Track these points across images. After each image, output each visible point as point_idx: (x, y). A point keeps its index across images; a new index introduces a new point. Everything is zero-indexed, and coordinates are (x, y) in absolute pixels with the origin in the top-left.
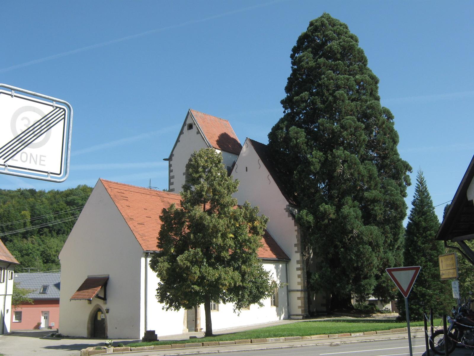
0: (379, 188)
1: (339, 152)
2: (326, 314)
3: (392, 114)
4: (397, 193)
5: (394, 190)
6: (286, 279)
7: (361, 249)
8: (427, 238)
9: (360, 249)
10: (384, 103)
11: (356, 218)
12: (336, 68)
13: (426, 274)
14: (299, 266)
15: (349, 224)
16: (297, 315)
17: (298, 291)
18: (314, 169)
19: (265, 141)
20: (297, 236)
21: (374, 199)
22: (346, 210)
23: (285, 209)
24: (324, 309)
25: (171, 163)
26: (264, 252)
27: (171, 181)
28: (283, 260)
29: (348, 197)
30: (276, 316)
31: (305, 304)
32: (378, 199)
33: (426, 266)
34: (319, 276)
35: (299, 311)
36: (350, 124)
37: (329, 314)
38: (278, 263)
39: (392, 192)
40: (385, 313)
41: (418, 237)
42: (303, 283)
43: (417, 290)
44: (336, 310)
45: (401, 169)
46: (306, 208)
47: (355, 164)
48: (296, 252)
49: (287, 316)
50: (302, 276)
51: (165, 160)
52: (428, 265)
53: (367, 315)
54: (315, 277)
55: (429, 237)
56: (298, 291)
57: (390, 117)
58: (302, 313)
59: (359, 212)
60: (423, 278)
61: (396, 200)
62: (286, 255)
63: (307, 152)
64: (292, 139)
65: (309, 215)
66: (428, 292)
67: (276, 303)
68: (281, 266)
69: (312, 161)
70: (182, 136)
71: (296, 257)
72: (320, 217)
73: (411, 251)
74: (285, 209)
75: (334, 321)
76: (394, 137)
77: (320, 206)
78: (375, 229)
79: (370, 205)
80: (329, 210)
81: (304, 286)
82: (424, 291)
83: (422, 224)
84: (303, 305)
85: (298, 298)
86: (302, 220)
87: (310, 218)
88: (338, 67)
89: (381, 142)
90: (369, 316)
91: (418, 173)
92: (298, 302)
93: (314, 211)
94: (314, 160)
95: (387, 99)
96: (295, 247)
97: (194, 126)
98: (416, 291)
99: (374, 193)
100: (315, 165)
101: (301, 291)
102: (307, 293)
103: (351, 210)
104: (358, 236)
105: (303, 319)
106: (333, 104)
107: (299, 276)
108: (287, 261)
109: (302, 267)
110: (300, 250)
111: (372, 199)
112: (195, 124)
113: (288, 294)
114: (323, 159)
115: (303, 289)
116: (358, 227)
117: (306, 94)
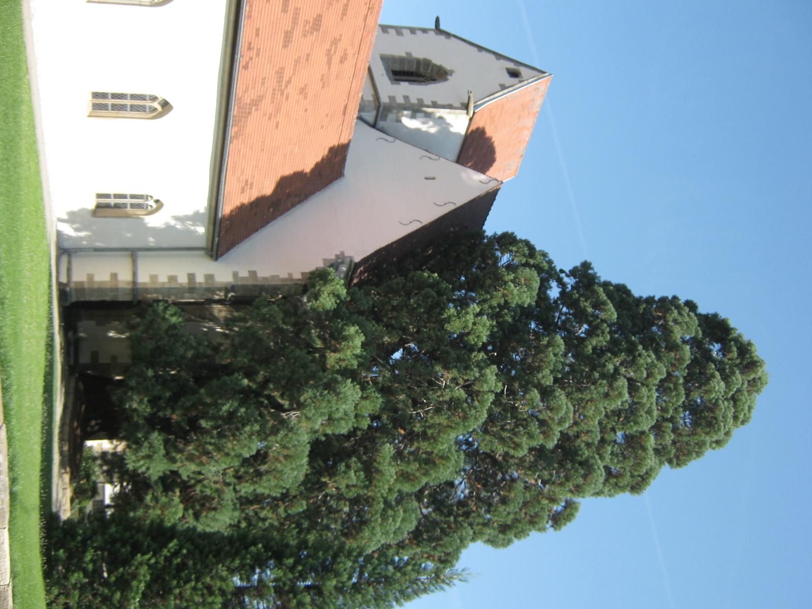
0: (398, 486)
1: (491, 380)
2: (72, 363)
3: (565, 524)
4: (386, 533)
5: (394, 525)
6: (165, 245)
7: (247, 428)
8: (291, 595)
9: (247, 424)
10: (587, 504)
11: (330, 419)
12: (670, 388)
13: (188, 592)
14: (200, 279)
15: (315, 397)
16: (69, 270)
17: (135, 274)
18: (449, 317)
19: (492, 226)
20: (278, 276)
21: (378, 471)
22: (350, 391)
23: (342, 253)
24: (85, 358)
25: (432, 34)
26: (238, 179)
27: (390, 30)
28: (216, 234)
29: (381, 400)
30: (69, 210)
31: (100, 290)
32: (374, 482)
33: (211, 593)
34: (174, 327)
35: (80, 276)
36: (559, 408)
37: (70, 370)
38: (209, 223)
39: (391, 519)
40: (71, 510)
41: (292, 569)
42: (154, 286)
43: (141, 564)
44: (81, 386)
45: (441, 546)
46: (348, 299)
47: (465, 418)
48: (235, 275)
49: (66, 245)
50: (173, 285)
51: (437, 21)
52: (213, 597)
53: (67, 459)
54: (172, 315)
55: (295, 601)
56: (135, 274)
57: (557, 520)
58: (75, 283)
59: (344, 429)
60: (175, 583)
61: (373, 528)
62: (228, 250)
63: (486, 306)
64: (514, 273)
65: (333, 300)
66: (134, 598)
67: (102, 210)
68: (201, 230)
69: (467, 313)
70: (493, 57)
71: (224, 273)
72: (332, 326)
73: (253, 548)
74: (342, 253)
75: (50, 365)
76: (517, 527)
77: (357, 328)
78: (294, 472)
79: (360, 459)
80: (348, 348)
81: (146, 290)
82: (138, 587)
83: (329, 579)
84: (96, 286)
85: (114, 276)
86: (321, 282)
87: (327, 302)
88: (672, 391)
89: (507, 494)
90: (62, 465)
91: (463, 570)
92: (104, 274)
93: (345, 312)
94: (470, 318)
95: (599, 512)
96: (249, 272)
97: (515, 80)
98: (136, 563)
99: (389, 471)
100: (459, 318)
101: (134, 282)
102: (128, 298)
103: (349, 407)
104: (283, 422)
105: (59, 284)
106: (599, 373)
107: (172, 278)
108: (212, 250)
109: (197, 286)
110: (240, 283)
111: (375, 464)
112: (521, 82)
113: (126, 249)
114: (472, 339)
115: (139, 286)
116: (306, 425)
117: (612, 313)
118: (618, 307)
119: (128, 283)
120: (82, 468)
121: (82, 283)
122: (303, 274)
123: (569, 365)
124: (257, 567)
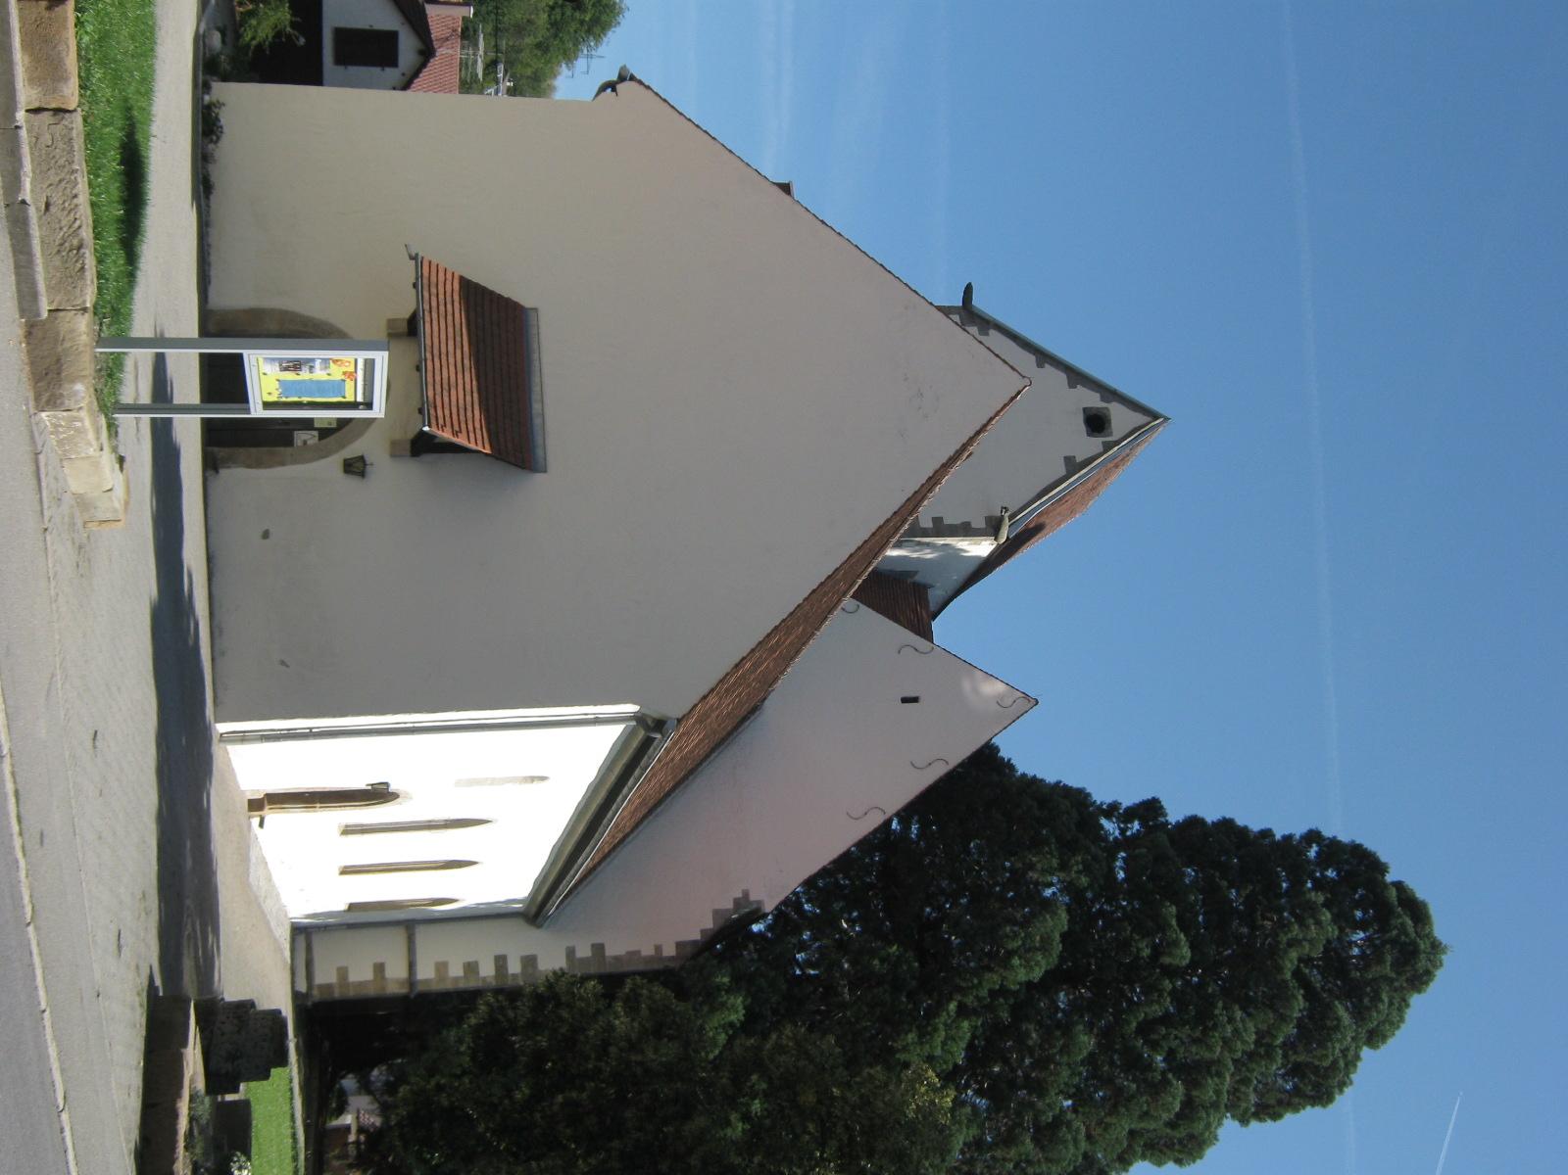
35: (326, 975)
48: (570, 953)
51: (968, 290)
58: (320, 987)
84: (351, 993)
118: (1192, 947)
119: (401, 983)
120: (1319, 990)
121: (329, 987)
122: (679, 945)
123: (1074, 1086)
124: (1027, 1056)
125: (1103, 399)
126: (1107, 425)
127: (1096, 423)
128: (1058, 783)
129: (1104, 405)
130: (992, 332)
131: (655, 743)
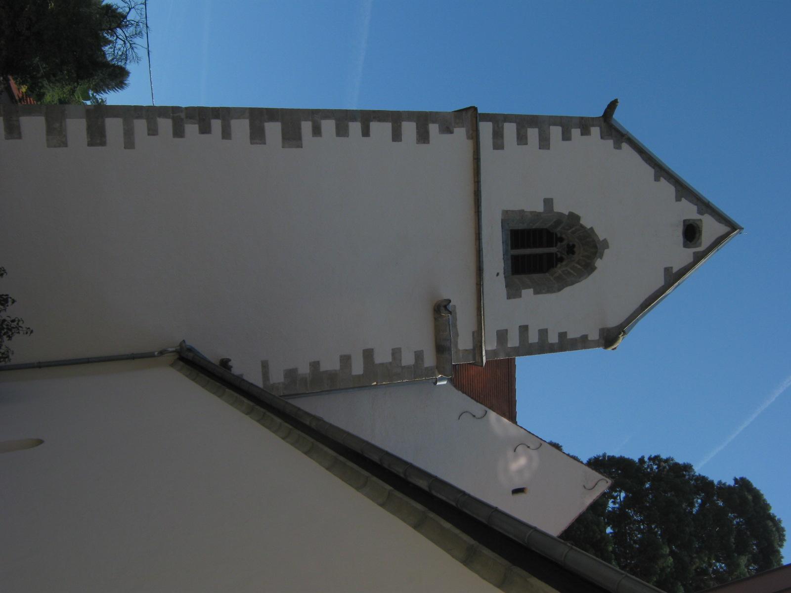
51: (613, 105)
125: (700, 212)
126: (697, 235)
127: (691, 233)
128: (632, 459)
129: (699, 217)
130: (625, 146)
131: (510, 247)
